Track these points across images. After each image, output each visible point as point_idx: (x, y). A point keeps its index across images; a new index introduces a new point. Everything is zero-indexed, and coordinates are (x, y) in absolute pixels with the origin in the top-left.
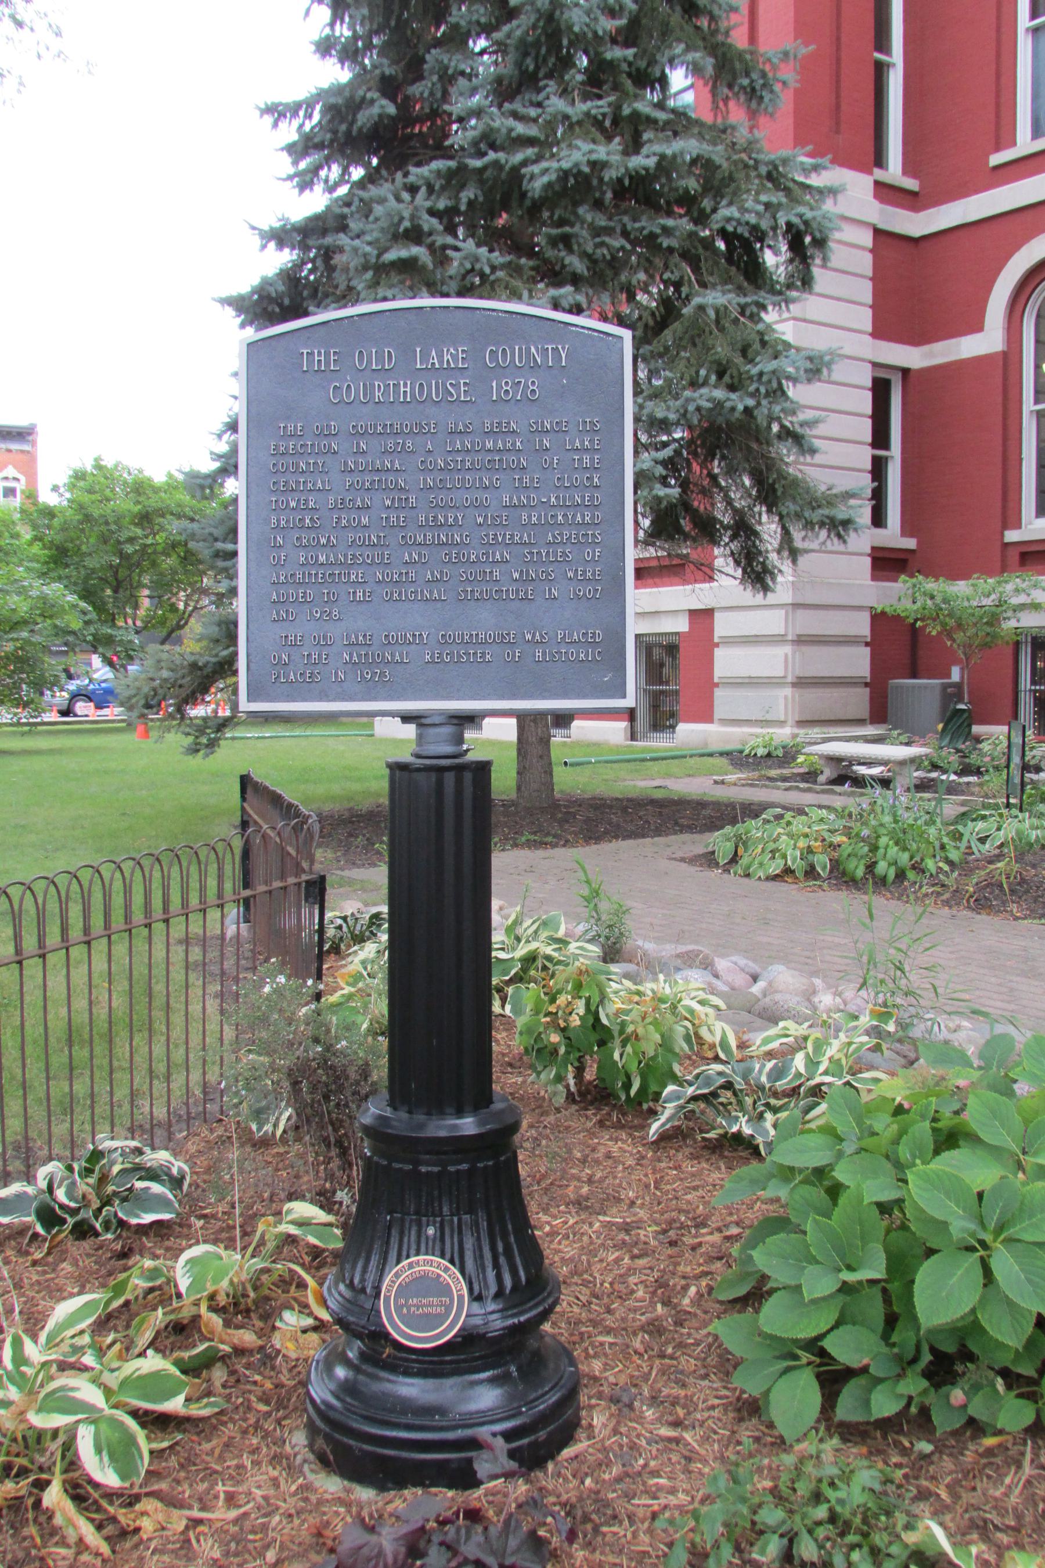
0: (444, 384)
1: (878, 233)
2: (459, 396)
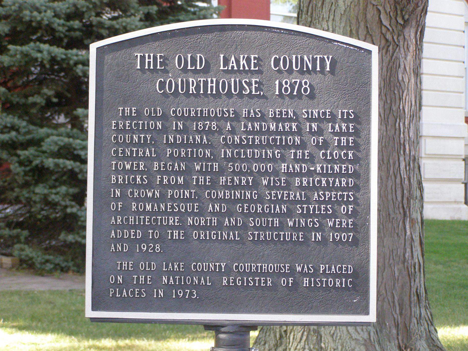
0: (240, 82)
2: (251, 91)
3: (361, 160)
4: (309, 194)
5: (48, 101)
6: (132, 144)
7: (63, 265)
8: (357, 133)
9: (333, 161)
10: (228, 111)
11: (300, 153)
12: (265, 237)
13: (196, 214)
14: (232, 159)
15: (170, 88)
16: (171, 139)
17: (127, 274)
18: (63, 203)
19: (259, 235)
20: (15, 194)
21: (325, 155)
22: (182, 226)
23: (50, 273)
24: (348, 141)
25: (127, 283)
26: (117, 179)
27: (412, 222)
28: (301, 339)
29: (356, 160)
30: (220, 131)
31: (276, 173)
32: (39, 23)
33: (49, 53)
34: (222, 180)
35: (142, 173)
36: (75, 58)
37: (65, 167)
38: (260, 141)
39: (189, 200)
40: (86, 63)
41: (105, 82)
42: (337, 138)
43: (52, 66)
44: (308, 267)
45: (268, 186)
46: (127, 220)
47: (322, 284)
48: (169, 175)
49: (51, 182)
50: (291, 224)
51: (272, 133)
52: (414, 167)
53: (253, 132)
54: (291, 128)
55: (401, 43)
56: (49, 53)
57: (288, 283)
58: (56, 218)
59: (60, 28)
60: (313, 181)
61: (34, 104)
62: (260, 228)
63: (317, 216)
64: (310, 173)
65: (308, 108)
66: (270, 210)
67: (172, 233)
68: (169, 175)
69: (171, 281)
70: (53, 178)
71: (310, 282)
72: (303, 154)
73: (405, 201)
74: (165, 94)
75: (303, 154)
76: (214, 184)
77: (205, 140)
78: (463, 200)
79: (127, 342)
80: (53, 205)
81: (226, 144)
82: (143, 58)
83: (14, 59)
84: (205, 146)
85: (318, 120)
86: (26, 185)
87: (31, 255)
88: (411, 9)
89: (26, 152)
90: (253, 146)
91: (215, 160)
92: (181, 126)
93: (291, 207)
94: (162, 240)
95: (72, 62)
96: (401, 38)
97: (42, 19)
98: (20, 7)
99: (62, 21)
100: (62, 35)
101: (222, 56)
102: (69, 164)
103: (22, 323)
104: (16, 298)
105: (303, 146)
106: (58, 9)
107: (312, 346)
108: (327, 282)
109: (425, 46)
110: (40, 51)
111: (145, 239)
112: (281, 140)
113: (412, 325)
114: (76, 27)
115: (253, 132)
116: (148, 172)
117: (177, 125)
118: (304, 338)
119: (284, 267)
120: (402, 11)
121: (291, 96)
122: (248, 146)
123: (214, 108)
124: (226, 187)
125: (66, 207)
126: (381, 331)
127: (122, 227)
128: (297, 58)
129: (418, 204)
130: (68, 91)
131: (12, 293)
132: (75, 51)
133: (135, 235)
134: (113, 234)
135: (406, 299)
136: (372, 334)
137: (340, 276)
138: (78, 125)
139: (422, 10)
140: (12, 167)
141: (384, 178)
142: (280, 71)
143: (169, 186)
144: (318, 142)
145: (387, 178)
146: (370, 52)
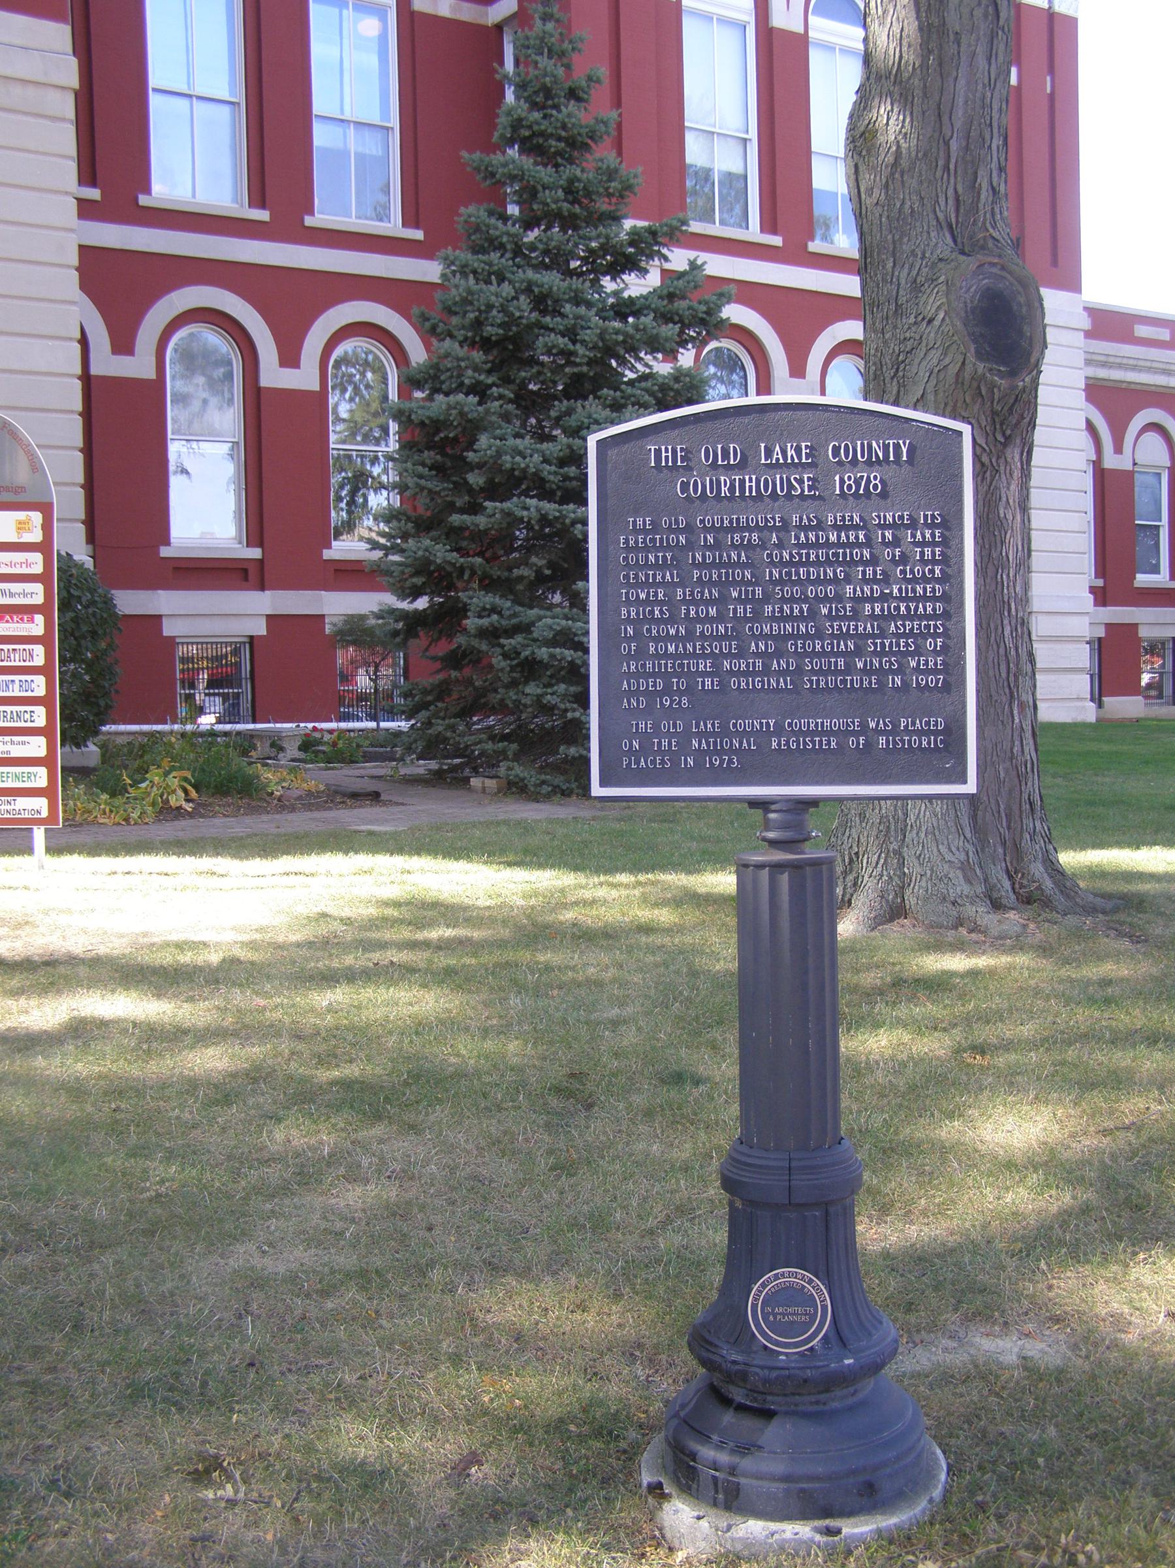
0: (788, 480)
1: (80, 201)
2: (803, 491)
3: (952, 577)
4: (883, 625)
5: (539, 572)
6: (647, 566)
7: (564, 787)
8: (945, 542)
9: (914, 580)
10: (773, 518)
11: (869, 571)
12: (827, 683)
13: (735, 656)
14: (780, 582)
15: (695, 491)
16: (699, 557)
17: (645, 738)
18: (562, 706)
19: (818, 681)
20: (499, 696)
21: (903, 572)
22: (716, 672)
23: (547, 797)
24: (933, 553)
25: (645, 750)
26: (629, 612)
27: (1022, 706)
28: (877, 863)
29: (944, 579)
30: (763, 545)
31: (839, 598)
32: (524, 471)
33: (538, 510)
34: (768, 609)
35: (661, 603)
36: (572, 515)
37: (563, 658)
38: (817, 556)
39: (725, 637)
40: (585, 522)
41: (609, 485)
42: (919, 550)
43: (542, 528)
44: (884, 722)
45: (829, 616)
46: (643, 666)
47: (904, 744)
48: (697, 606)
49: (545, 680)
50: (860, 665)
51: (833, 545)
52: (1023, 633)
53: (807, 545)
54: (857, 538)
55: (1002, 468)
56: (538, 510)
57: (858, 743)
58: (553, 727)
59: (552, 478)
60: (889, 608)
61: (521, 578)
62: (820, 672)
63: (894, 654)
64: (884, 598)
65: (879, 511)
66: (833, 648)
67: (703, 682)
68: (697, 606)
69: (704, 745)
70: (548, 673)
71: (888, 742)
72: (875, 572)
73: (1012, 679)
74: (688, 498)
75: (875, 572)
76: (757, 616)
77: (743, 558)
78: (1089, 696)
79: (650, 876)
80: (548, 709)
81: (772, 563)
82: (658, 452)
83: (492, 520)
84: (744, 566)
85: (893, 526)
86: (514, 684)
87: (521, 775)
88: (1014, 421)
89: (512, 641)
90: (808, 563)
91: (757, 584)
92: (710, 539)
93: (860, 643)
94: (690, 691)
95: (567, 521)
96: (1002, 461)
97: (528, 466)
98: (497, 451)
99: (553, 468)
100: (554, 486)
101: (763, 445)
102: (569, 654)
103: (511, 858)
104: (504, 829)
105: (874, 561)
106: (548, 452)
107: (892, 873)
108: (910, 741)
109: (1035, 472)
110: (527, 509)
111: (667, 691)
112: (845, 554)
113: (1024, 842)
114: (572, 475)
115: (807, 545)
116: (669, 601)
117: (705, 538)
118: (882, 861)
119: (853, 723)
120: (1002, 424)
121: (856, 495)
122: (801, 564)
123: (755, 517)
124: (773, 618)
125: (566, 711)
126: (983, 851)
127: (637, 675)
128: (862, 445)
129: (1029, 683)
130: (565, 560)
131: (498, 823)
132: (571, 506)
133: (654, 685)
134: (625, 685)
135: (1015, 808)
136: (971, 854)
137: (928, 733)
138: (579, 602)
139: (1029, 423)
140: (494, 661)
141: (983, 649)
142: (840, 463)
143: (698, 619)
144: (894, 555)
145: (988, 648)
146: (960, 433)
